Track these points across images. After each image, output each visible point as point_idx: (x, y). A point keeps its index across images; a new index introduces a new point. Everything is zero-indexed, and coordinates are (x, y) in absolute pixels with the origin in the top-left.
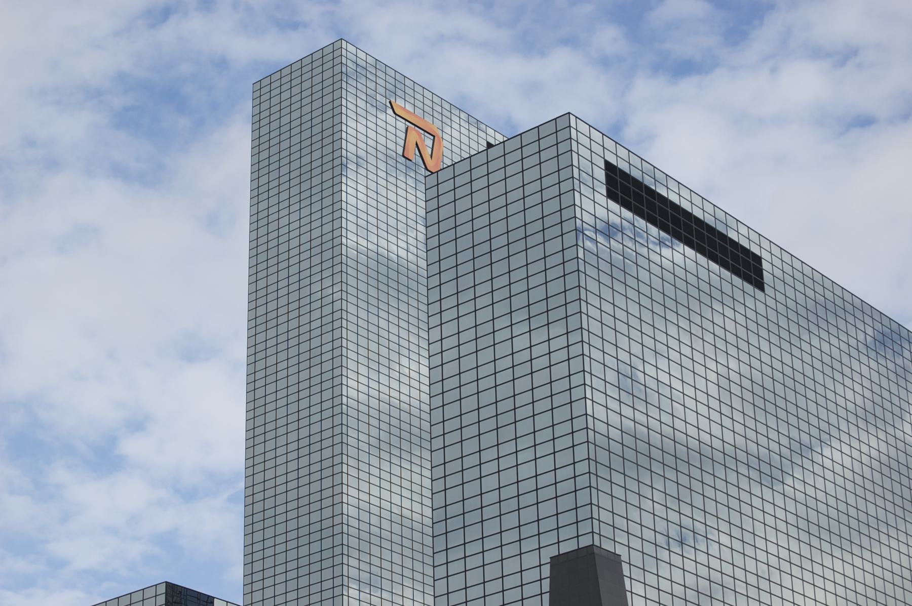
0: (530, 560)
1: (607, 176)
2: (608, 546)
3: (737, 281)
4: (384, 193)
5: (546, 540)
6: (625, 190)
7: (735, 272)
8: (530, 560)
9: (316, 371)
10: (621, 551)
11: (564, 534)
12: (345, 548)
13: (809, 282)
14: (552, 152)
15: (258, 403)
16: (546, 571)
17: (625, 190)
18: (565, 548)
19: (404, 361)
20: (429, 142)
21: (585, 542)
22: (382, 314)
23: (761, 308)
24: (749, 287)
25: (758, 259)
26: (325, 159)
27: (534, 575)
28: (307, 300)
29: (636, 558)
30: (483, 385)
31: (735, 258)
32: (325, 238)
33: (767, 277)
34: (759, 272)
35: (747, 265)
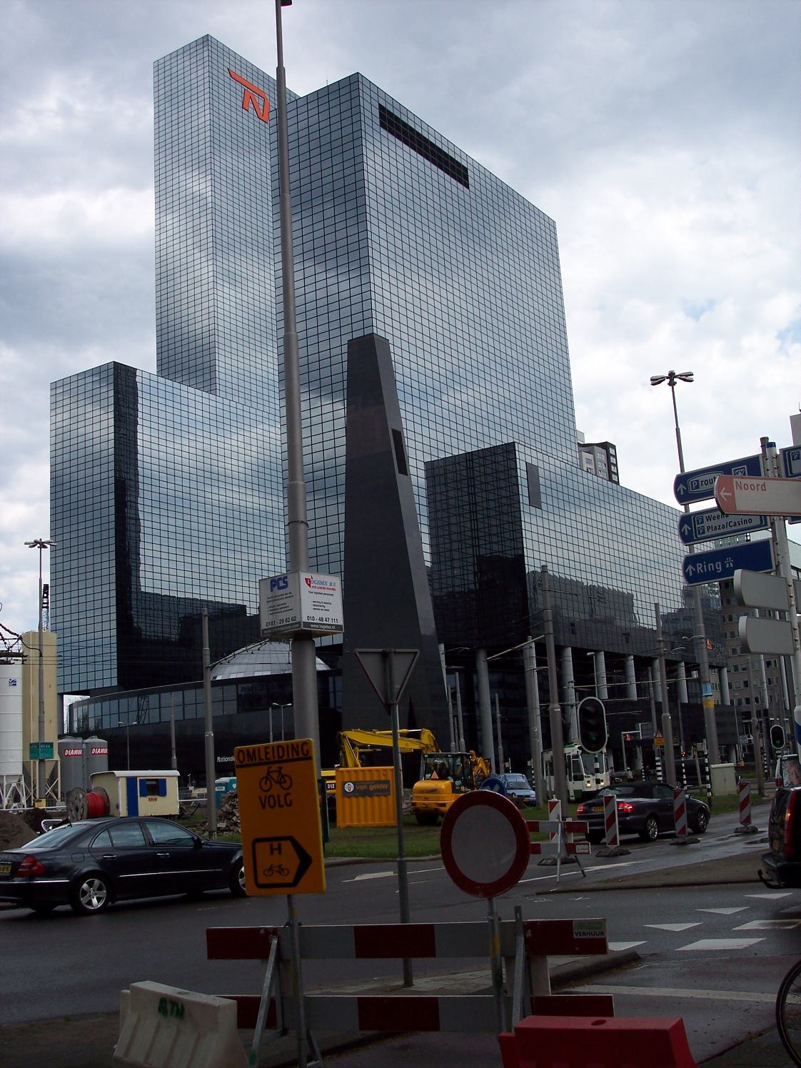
0: (335, 343)
1: (380, 114)
2: (381, 334)
3: (434, 167)
4: (224, 141)
5: (345, 330)
6: (391, 123)
7: (453, 176)
8: (335, 343)
10: (389, 337)
11: (355, 326)
12: (217, 343)
13: (482, 176)
14: (348, 97)
15: (162, 193)
16: (345, 348)
17: (391, 123)
18: (356, 335)
19: (250, 284)
20: (262, 102)
21: (367, 331)
22: (231, 253)
23: (467, 199)
24: (460, 186)
25: (466, 170)
26: (176, 79)
27: (338, 351)
28: (174, 160)
29: (397, 342)
30: (319, 285)
31: (420, 144)
32: (187, 117)
34: (466, 177)
35: (459, 173)
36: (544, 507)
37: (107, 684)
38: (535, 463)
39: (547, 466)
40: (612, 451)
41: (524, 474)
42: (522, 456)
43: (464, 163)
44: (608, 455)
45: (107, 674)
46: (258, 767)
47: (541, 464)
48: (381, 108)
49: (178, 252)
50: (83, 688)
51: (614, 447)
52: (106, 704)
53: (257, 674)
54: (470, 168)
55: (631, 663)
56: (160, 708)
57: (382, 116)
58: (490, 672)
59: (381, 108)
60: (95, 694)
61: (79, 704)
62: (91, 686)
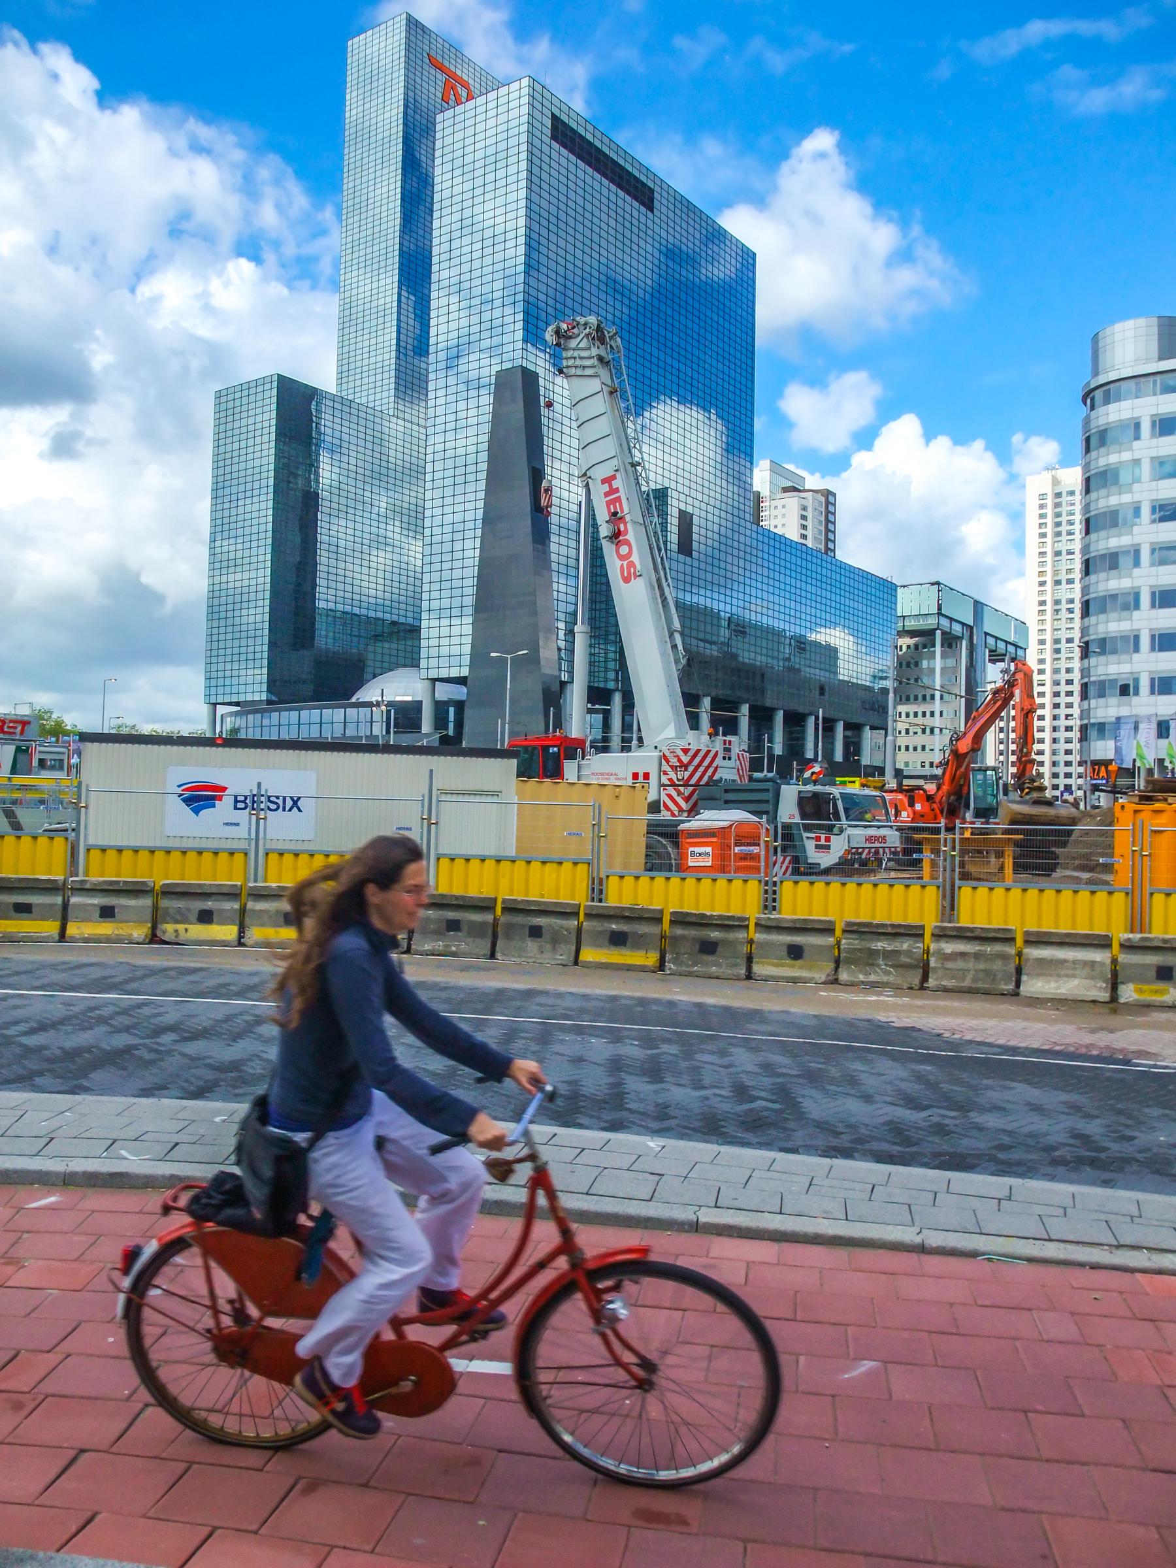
1: (652, 202)
9: (383, 245)
23: (650, 224)
24: (643, 209)
25: (652, 191)
33: (656, 204)
36: (695, 554)
37: (257, 697)
38: (690, 509)
39: (703, 514)
40: (831, 499)
41: (675, 521)
42: (675, 503)
43: (651, 184)
44: (828, 503)
45: (257, 688)
46: (175, 749)
47: (697, 512)
48: (554, 118)
49: (459, 198)
50: (235, 699)
51: (834, 495)
52: (250, 717)
53: (398, 699)
54: (657, 189)
55: (779, 717)
56: (321, 723)
57: (554, 128)
58: (845, 729)
59: (554, 118)
60: (246, 708)
61: (231, 714)
62: (242, 698)
